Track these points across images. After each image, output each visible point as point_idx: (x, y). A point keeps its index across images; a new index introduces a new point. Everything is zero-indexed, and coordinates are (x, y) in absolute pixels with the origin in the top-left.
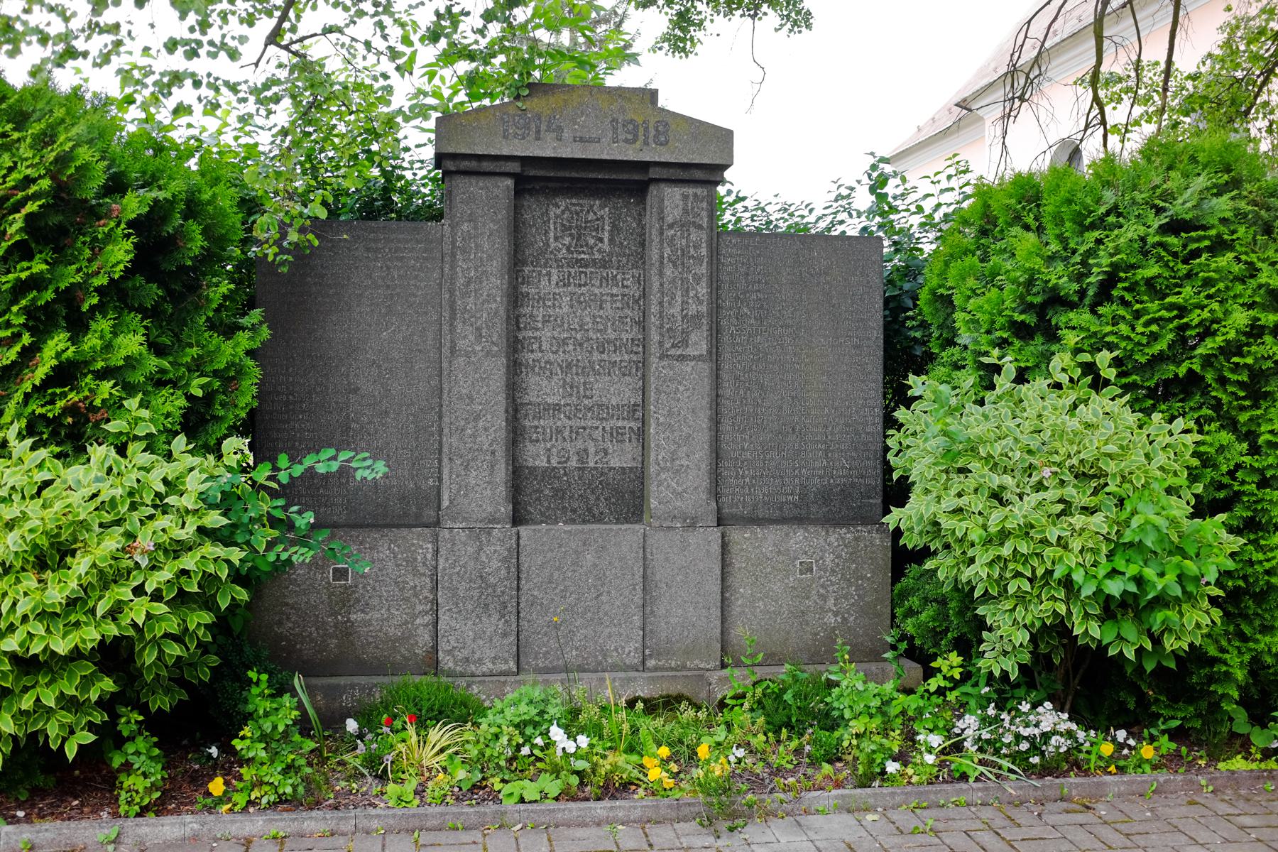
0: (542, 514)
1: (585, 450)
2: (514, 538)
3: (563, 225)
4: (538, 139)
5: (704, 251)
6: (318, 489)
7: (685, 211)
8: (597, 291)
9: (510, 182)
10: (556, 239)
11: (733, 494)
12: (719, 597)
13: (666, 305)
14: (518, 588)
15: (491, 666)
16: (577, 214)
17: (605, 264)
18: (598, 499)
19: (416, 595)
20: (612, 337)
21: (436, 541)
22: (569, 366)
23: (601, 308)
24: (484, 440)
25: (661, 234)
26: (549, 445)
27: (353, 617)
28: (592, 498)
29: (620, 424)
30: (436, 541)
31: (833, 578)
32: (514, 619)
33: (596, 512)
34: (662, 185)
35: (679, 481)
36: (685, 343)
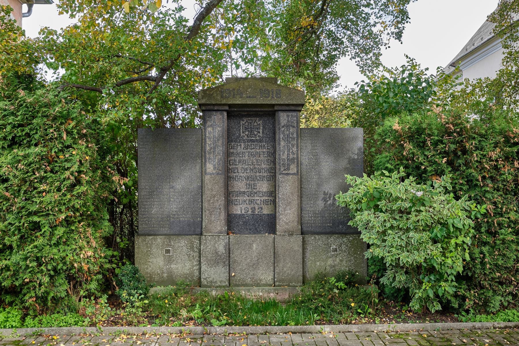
0: (239, 231)
1: (254, 208)
2: (228, 238)
3: (245, 127)
4: (233, 97)
5: (295, 136)
6: (160, 222)
7: (288, 121)
8: (258, 151)
9: (225, 114)
10: (243, 132)
11: (308, 223)
12: (302, 260)
13: (281, 155)
14: (229, 257)
15: (219, 284)
16: (250, 123)
17: (261, 141)
18: (259, 225)
19: (194, 259)
20: (264, 167)
21: (200, 240)
22: (248, 178)
23: (260, 157)
24: (217, 205)
25: (280, 130)
26: (241, 206)
27: (172, 266)
28: (257, 225)
29: (267, 198)
30: (200, 240)
31: (345, 254)
32: (228, 267)
33: (258, 230)
34: (280, 112)
35: (287, 217)
36: (288, 169)
